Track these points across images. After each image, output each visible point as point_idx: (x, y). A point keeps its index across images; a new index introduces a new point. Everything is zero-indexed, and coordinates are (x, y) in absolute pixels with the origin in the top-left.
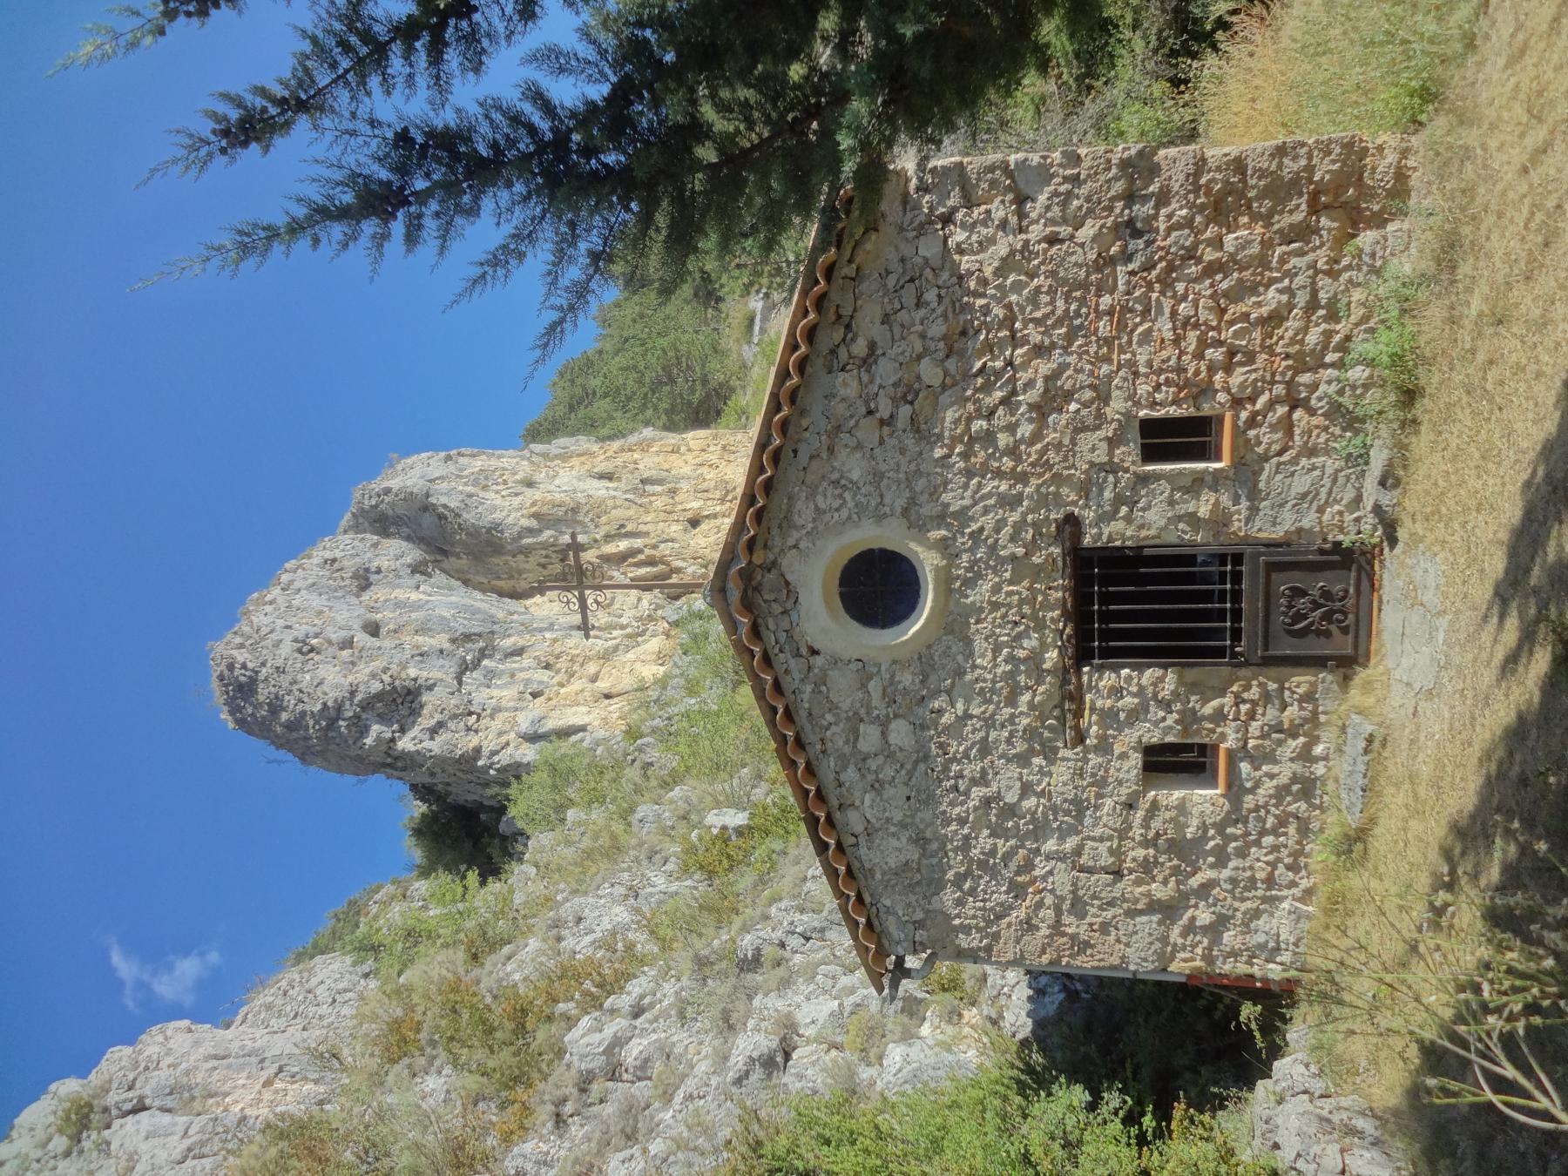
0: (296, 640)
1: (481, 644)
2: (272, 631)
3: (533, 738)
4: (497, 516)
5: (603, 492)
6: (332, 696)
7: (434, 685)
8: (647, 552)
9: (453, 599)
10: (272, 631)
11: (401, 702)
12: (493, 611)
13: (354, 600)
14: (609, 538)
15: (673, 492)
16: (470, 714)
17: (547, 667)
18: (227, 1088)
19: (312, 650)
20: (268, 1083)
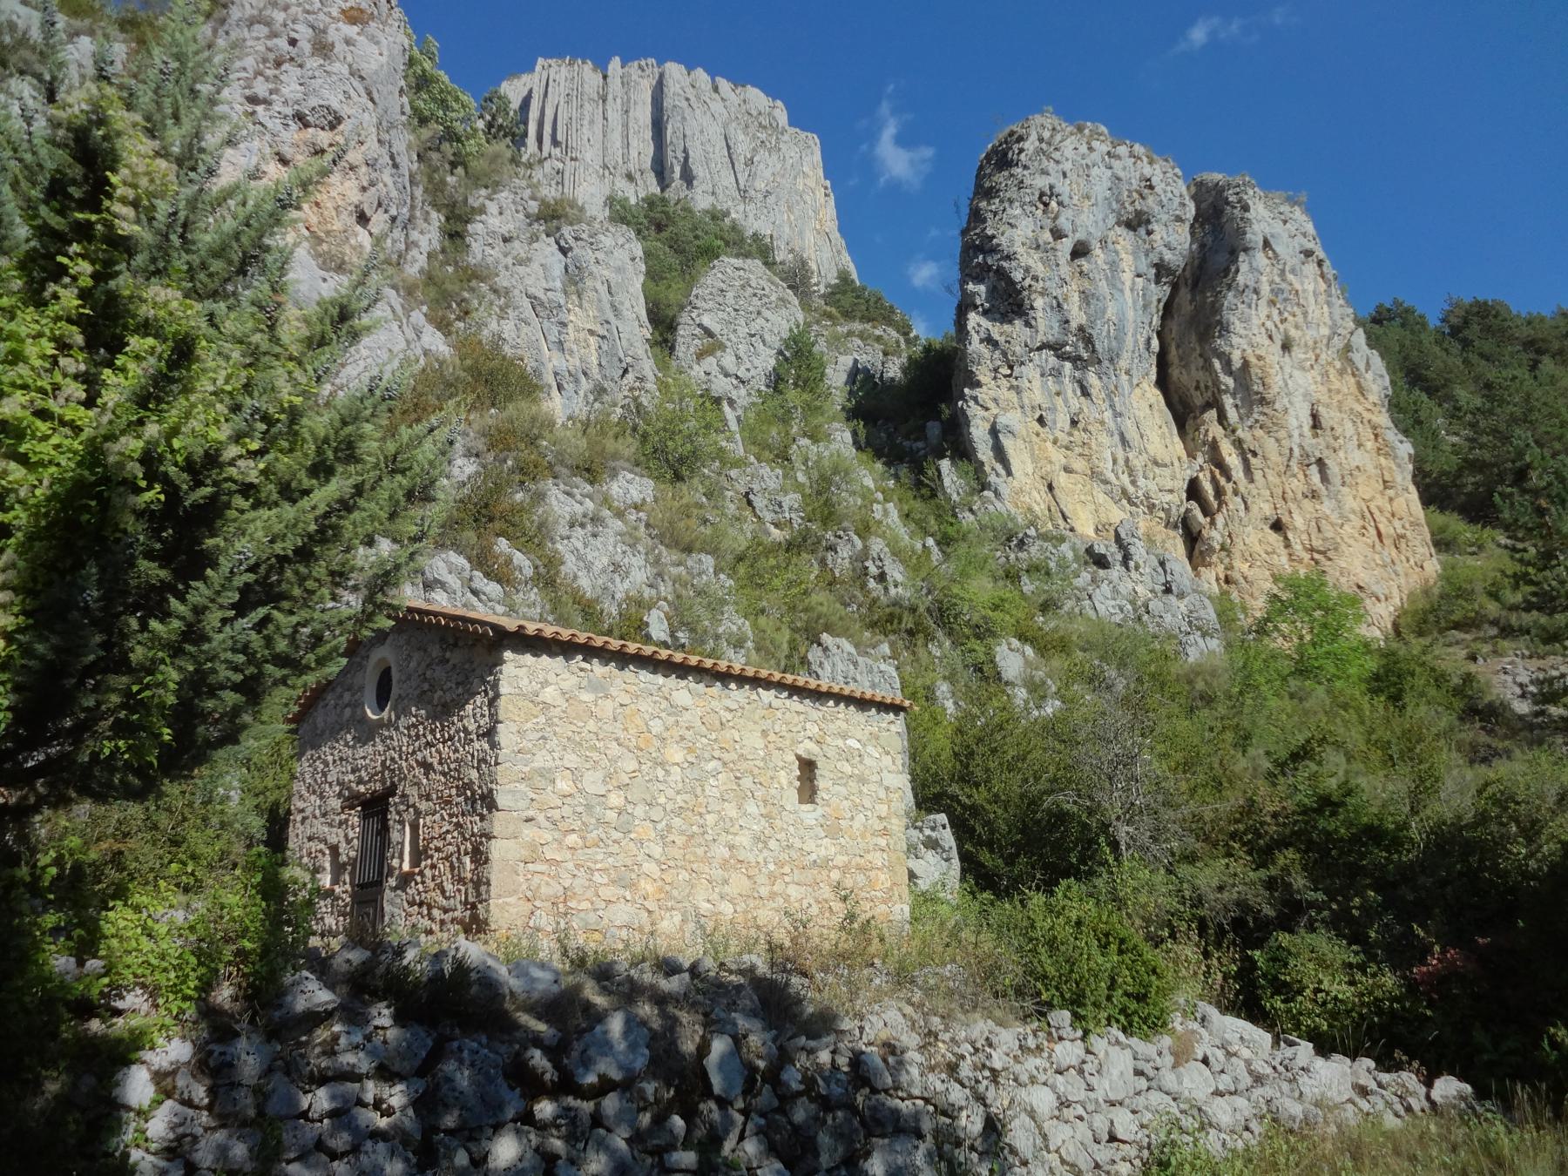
0: (1051, 187)
1: (1086, 356)
2: (1058, 162)
3: (994, 432)
4: (1238, 326)
5: (1293, 423)
6: (1002, 241)
7: (1031, 326)
8: (1229, 487)
9: (1130, 314)
10: (1058, 162)
11: (1010, 302)
12: (1125, 355)
13: (1112, 220)
14: (1238, 444)
15: (1314, 495)
16: (1011, 367)
17: (1074, 423)
18: (585, 304)
19: (1046, 205)
20: (591, 332)
